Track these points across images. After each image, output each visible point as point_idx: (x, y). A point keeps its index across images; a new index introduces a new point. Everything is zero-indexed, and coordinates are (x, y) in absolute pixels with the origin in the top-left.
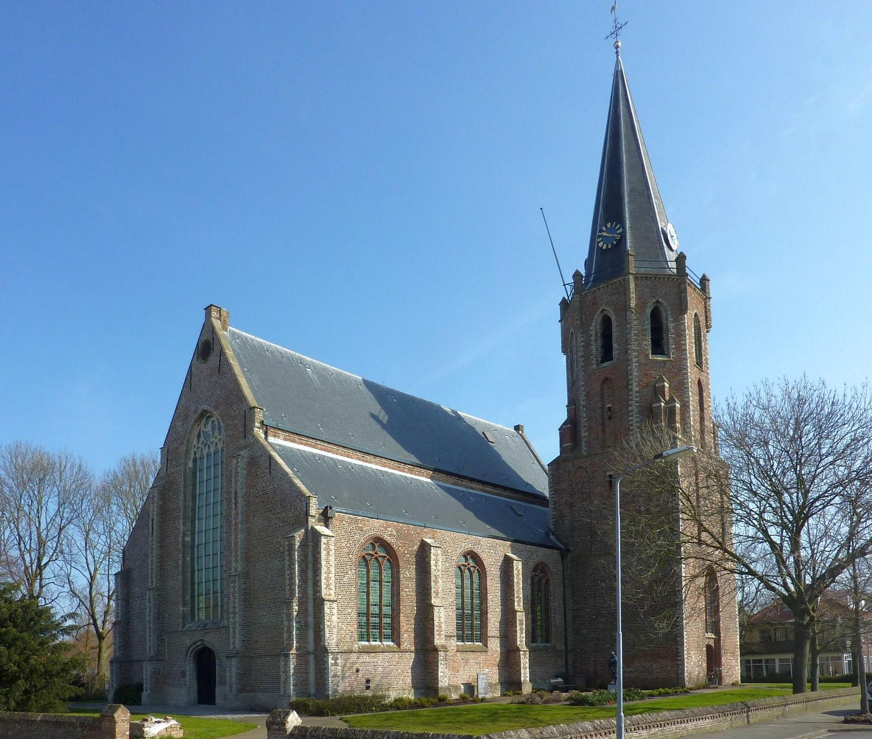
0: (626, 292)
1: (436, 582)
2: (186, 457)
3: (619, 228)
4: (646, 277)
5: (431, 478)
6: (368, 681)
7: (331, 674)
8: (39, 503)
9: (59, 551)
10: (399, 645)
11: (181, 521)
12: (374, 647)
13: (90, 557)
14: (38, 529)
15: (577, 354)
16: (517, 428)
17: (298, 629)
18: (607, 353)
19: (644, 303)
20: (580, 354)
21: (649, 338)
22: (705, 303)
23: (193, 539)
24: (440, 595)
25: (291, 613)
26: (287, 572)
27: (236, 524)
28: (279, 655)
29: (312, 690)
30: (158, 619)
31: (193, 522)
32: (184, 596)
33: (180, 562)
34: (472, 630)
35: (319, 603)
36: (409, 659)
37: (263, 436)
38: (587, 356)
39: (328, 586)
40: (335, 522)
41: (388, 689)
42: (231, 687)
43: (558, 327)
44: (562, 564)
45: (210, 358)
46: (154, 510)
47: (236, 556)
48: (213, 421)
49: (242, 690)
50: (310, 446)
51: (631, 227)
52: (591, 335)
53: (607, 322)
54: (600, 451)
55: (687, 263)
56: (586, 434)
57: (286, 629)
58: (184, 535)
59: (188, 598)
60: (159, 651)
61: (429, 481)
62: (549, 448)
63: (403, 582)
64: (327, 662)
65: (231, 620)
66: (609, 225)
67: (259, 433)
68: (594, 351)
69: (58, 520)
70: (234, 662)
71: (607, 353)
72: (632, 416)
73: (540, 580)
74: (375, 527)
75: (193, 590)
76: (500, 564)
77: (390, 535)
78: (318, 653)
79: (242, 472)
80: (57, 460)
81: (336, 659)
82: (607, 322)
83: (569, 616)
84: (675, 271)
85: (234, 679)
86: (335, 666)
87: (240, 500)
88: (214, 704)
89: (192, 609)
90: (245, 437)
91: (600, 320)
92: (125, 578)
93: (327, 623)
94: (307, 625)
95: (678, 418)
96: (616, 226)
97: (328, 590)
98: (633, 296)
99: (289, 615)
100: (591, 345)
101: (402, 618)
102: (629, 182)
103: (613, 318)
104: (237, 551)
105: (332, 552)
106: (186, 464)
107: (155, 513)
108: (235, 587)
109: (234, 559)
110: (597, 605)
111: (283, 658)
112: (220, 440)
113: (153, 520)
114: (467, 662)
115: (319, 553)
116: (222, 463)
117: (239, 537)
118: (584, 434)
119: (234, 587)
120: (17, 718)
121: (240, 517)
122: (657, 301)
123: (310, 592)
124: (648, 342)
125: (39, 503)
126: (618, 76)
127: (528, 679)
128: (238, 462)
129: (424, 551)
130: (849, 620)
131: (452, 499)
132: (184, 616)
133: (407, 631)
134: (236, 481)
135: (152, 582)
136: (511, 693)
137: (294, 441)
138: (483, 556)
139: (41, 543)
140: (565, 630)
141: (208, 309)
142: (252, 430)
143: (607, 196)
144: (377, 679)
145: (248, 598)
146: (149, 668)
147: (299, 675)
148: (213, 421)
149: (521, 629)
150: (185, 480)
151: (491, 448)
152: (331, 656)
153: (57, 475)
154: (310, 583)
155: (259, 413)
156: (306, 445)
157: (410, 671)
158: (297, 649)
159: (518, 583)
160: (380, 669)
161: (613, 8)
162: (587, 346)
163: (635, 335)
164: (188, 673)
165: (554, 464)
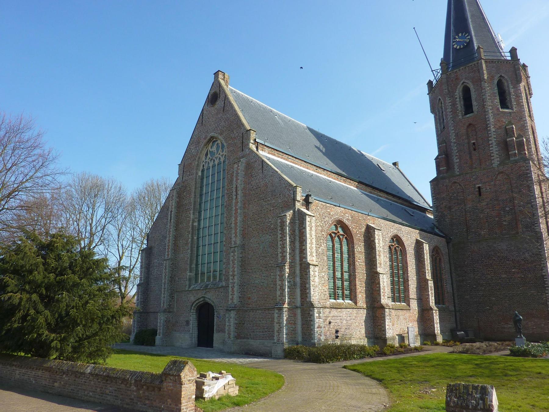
0: (479, 70)
1: (380, 256)
2: (197, 169)
3: (468, 36)
4: (492, 61)
5: (357, 187)
6: (337, 332)
7: (316, 325)
8: (93, 209)
9: (102, 241)
10: (356, 303)
11: (192, 212)
12: (340, 304)
13: (120, 245)
14: (91, 225)
16: (395, 164)
17: (289, 287)
18: (468, 108)
19: (493, 77)
21: (498, 98)
22: (527, 80)
23: (199, 224)
24: (382, 265)
25: (284, 275)
26: (280, 243)
27: (236, 210)
28: (274, 308)
29: (300, 339)
30: (171, 281)
31: (200, 213)
33: (190, 240)
34: (399, 294)
35: (305, 267)
36: (362, 314)
39: (311, 253)
40: (312, 206)
41: (350, 339)
42: (229, 334)
45: (217, 103)
46: (173, 204)
47: (236, 233)
48: (218, 144)
49: (238, 337)
50: (284, 159)
51: (475, 35)
52: (456, 98)
53: (466, 92)
54: (469, 171)
56: (458, 160)
57: (278, 287)
58: (193, 221)
59: (194, 266)
60: (170, 305)
61: (356, 189)
63: (357, 255)
64: (313, 315)
65: (231, 281)
66: (460, 35)
68: (459, 108)
69: (103, 220)
70: (233, 314)
71: (468, 108)
74: (338, 212)
75: (197, 261)
76: (413, 246)
77: (348, 219)
78: (305, 308)
79: (241, 173)
80: (107, 183)
81: (319, 313)
82: (466, 92)
84: (509, 58)
85: (232, 328)
86: (320, 320)
87: (239, 192)
89: (197, 274)
90: (243, 150)
91: (461, 89)
92: (148, 254)
93: (312, 283)
94: (295, 284)
97: (311, 258)
98: (485, 72)
99: (282, 276)
100: (457, 104)
101: (357, 282)
102: (470, 11)
105: (313, 229)
106: (197, 173)
107: (173, 207)
108: (236, 256)
109: (234, 235)
111: (277, 311)
112: (222, 156)
113: (171, 211)
114: (398, 317)
115: (305, 228)
116: (224, 170)
117: (239, 218)
118: (456, 160)
119: (234, 255)
120: (65, 368)
121: (239, 204)
122: (501, 76)
123: (298, 258)
124: (497, 100)
125: (93, 209)
127: (439, 332)
128: (238, 166)
129: (369, 233)
131: (372, 201)
133: (360, 292)
134: (237, 179)
135: (168, 255)
136: (429, 343)
137: (274, 155)
138: (404, 239)
139: (92, 235)
140: (453, 296)
141: (216, 74)
142: (248, 145)
144: (343, 330)
145: (244, 265)
146: (162, 318)
147: (289, 325)
148: (218, 144)
149: (432, 294)
150: (196, 184)
151: (384, 174)
152: (316, 310)
153: (105, 192)
154: (297, 252)
155: (253, 134)
156: (282, 158)
157: (363, 324)
158: (289, 304)
159: (427, 259)
160: (345, 322)
162: (454, 105)
163: (489, 96)
164: (191, 322)
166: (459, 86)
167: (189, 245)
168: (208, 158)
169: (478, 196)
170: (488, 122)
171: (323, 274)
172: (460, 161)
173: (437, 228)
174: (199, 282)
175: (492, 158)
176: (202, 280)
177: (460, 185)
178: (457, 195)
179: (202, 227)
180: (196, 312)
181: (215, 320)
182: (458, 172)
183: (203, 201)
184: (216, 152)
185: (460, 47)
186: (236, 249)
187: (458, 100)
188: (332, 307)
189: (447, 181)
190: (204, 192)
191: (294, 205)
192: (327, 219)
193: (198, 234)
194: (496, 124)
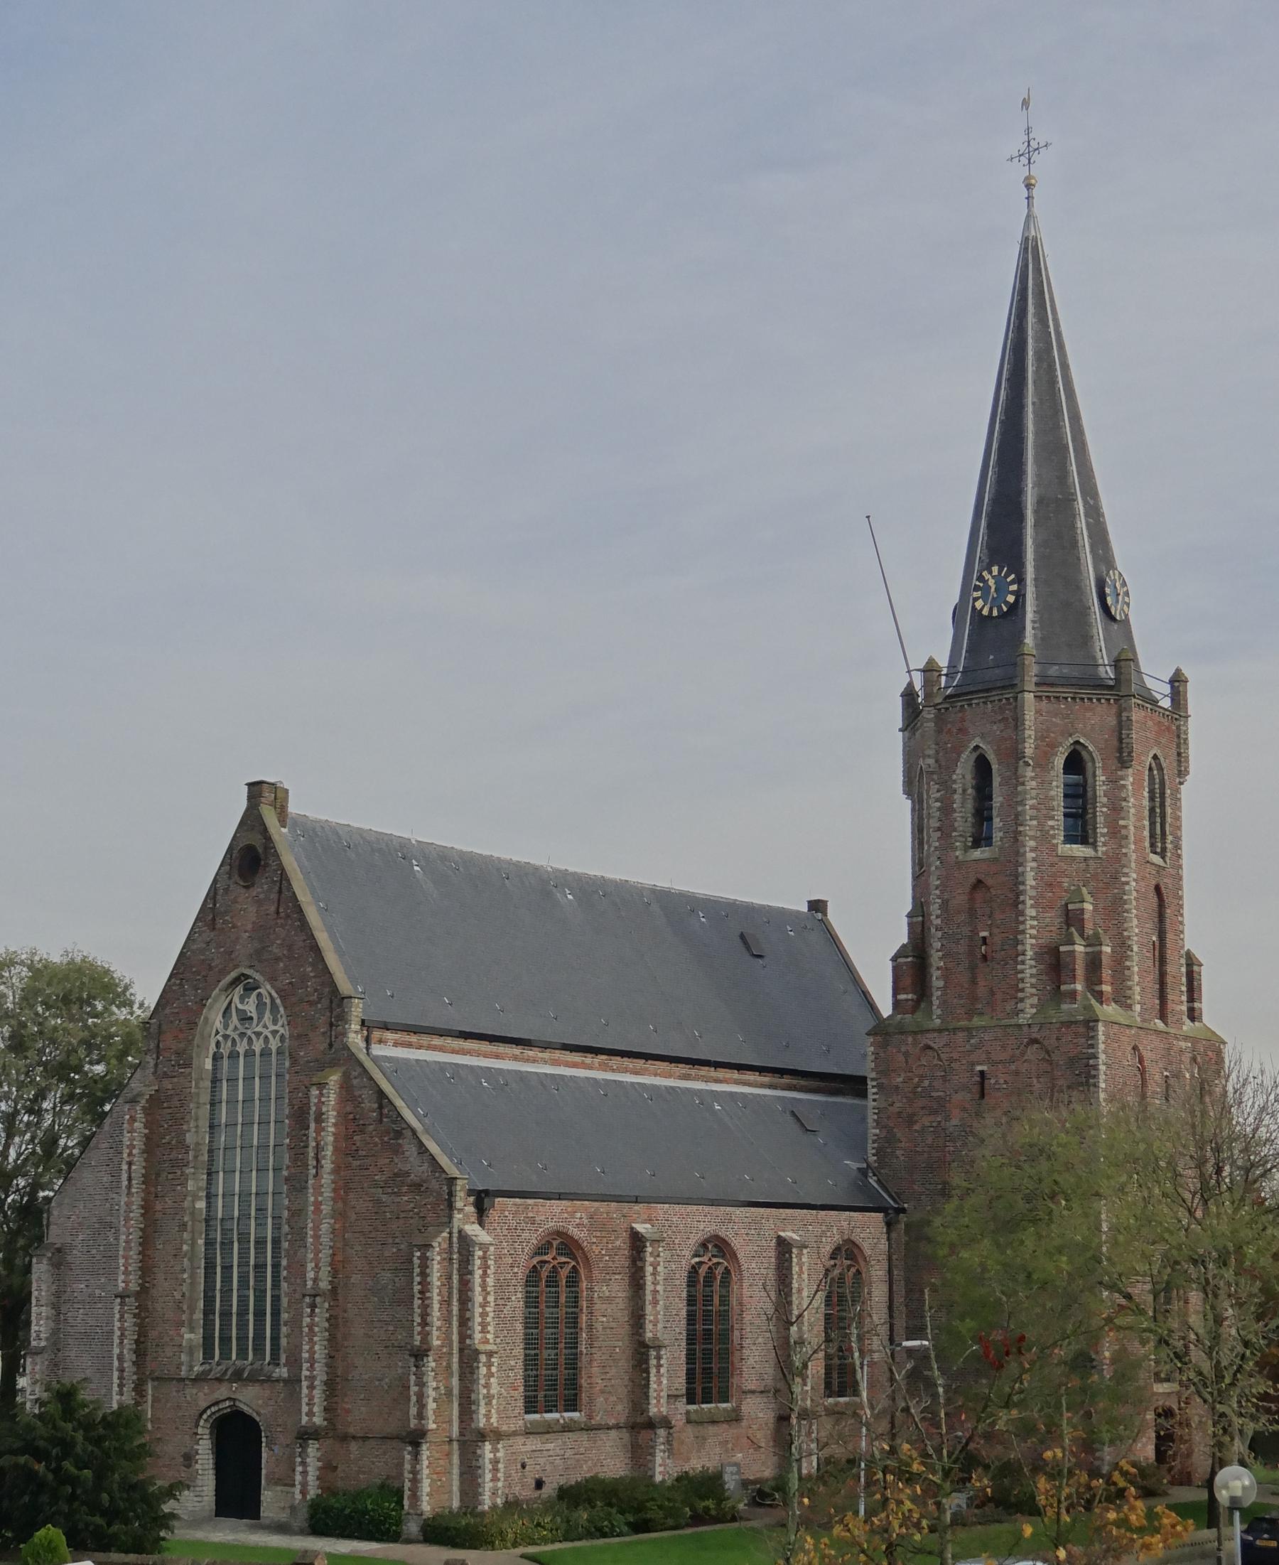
20: (934, 823)
37: (363, 1045)
38: (945, 831)
40: (493, 1215)
53: (982, 768)
66: (995, 569)
67: (355, 1039)
72: (1023, 963)
88: (258, 1517)
91: (972, 763)
94: (449, 1393)
95: (1106, 973)
96: (1007, 575)
98: (1030, 733)
103: (995, 767)
112: (274, 1033)
118: (936, 981)
123: (455, 1337)
124: (1057, 822)
126: (1030, 253)
130: (1175, 1455)
138: (736, 1243)
141: (256, 789)
142: (344, 1034)
143: (995, 501)
148: (259, 995)
161: (1026, 103)
162: (947, 810)
163: (1032, 807)
166: (964, 756)
168: (231, 1027)
170: (1021, 887)
174: (217, 1358)
175: (1020, 995)
176: (225, 1355)
180: (211, 1434)
181: (264, 1455)
184: (254, 1015)
185: (1000, 608)
186: (318, 1299)
188: (529, 1432)
189: (910, 1039)
191: (451, 1217)
192: (526, 1235)
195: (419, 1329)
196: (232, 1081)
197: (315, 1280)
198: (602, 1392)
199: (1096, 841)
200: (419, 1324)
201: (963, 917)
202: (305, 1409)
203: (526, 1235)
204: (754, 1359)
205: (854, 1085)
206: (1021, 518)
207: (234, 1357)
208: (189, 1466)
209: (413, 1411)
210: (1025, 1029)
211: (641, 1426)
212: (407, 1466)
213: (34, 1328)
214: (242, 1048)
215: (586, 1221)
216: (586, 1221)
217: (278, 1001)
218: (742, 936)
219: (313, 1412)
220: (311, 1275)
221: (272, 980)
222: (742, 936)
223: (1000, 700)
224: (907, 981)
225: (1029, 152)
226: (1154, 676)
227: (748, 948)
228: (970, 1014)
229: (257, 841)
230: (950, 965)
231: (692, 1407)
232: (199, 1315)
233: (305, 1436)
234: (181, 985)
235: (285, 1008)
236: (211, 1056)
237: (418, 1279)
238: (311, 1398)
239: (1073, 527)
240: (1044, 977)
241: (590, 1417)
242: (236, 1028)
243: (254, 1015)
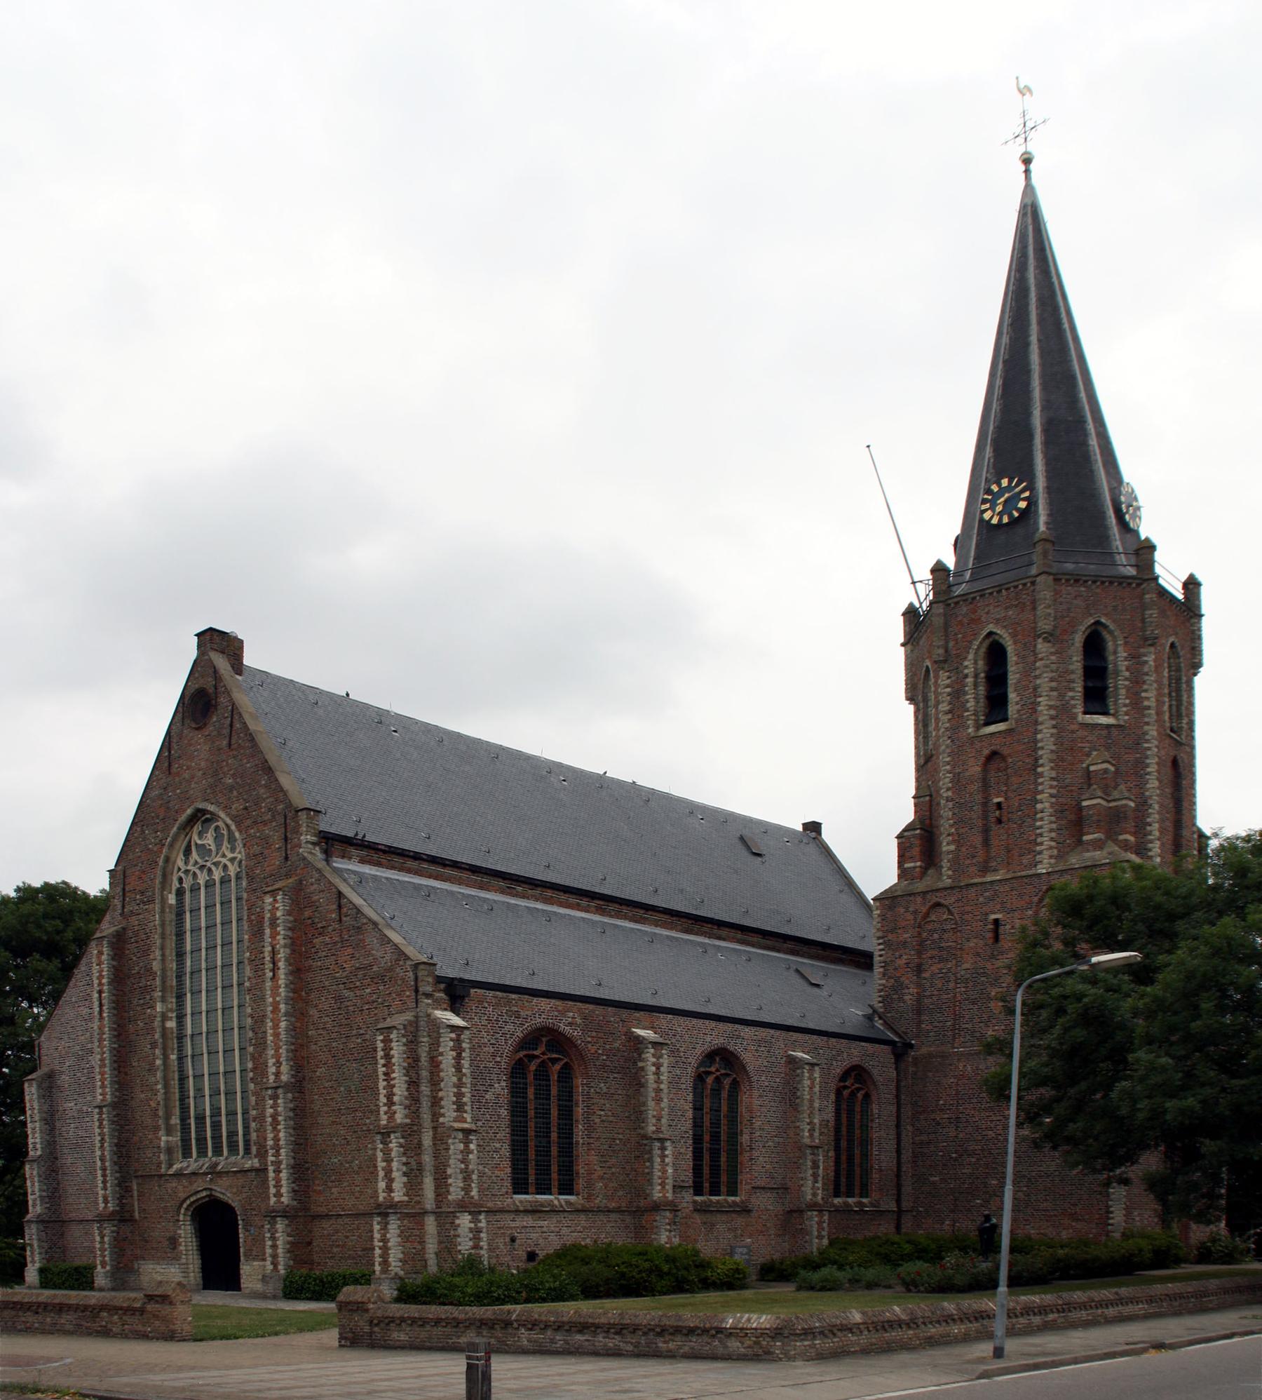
15: (936, 706)
18: (996, 705)
20: (944, 707)
31: (180, 997)
32: (168, 1117)
33: (158, 1062)
38: (957, 709)
40: (471, 1005)
43: (900, 653)
44: (896, 1069)
50: (409, 871)
52: (966, 676)
53: (996, 654)
55: (1158, 556)
56: (952, 847)
60: (121, 1205)
62: (874, 867)
65: (271, 1158)
66: (1005, 482)
68: (971, 704)
71: (996, 705)
73: (853, 1094)
77: (570, 1024)
82: (996, 654)
83: (907, 1155)
88: (239, 1289)
100: (965, 693)
103: (1010, 649)
104: (277, 1049)
106: (164, 900)
110: (961, 1136)
112: (232, 860)
118: (946, 847)
122: (1098, 623)
123: (426, 1117)
126: (1029, 189)
132: (169, 1151)
137: (379, 864)
148: (217, 828)
154: (425, 1103)
156: (401, 869)
162: (957, 694)
165: (888, 898)
167: (159, 1075)
168: (192, 861)
169: (991, 941)
171: (498, 1145)
172: (958, 849)
173: (880, 1018)
175: (1038, 848)
177: (950, 913)
178: (941, 938)
179: (189, 1032)
182: (949, 877)
183: (188, 970)
184: (213, 848)
185: (1010, 515)
186: (280, 1091)
187: (970, 680)
190: (188, 948)
192: (510, 1027)
193: (181, 1048)
194: (1063, 760)
195: (385, 1108)
196: (195, 911)
197: (277, 1074)
198: (601, 1178)
199: (1117, 712)
200: (385, 1105)
201: (975, 787)
202: (273, 1190)
203: (510, 1027)
204: (759, 1162)
205: (860, 960)
206: (1031, 436)
207: (210, 1154)
208: (174, 1248)
209: (382, 1185)
210: (1044, 878)
211: (641, 1210)
212: (377, 1236)
213: (30, 1141)
214: (202, 878)
215: (579, 1021)
216: (579, 1021)
217: (233, 827)
218: (742, 838)
219: (281, 1190)
220: (273, 1070)
221: (226, 808)
222: (742, 838)
223: (1016, 587)
224: (916, 851)
225: (1026, 130)
226: (1170, 577)
227: (748, 848)
228: (985, 870)
229: (209, 683)
230: (961, 831)
231: (698, 1198)
232: (175, 1120)
233: (272, 1215)
234: (143, 832)
235: (240, 832)
236: (174, 891)
237: (382, 1062)
238: (278, 1180)
239: (1084, 444)
240: (1065, 832)
241: (589, 1198)
242: (196, 863)
243: (213, 848)
